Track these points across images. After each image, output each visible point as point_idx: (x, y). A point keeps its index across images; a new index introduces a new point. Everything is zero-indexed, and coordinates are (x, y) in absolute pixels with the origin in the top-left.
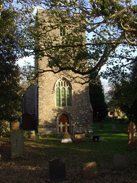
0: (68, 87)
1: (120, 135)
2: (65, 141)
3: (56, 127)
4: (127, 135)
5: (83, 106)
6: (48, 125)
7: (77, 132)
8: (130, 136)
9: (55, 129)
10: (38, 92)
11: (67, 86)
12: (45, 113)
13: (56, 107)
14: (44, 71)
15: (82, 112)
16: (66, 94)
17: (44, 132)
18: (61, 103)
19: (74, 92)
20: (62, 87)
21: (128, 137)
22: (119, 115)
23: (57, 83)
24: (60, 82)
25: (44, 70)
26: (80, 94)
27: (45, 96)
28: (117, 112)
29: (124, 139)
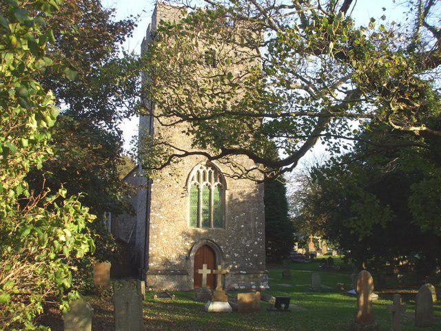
0: (217, 183)
1: (331, 296)
2: (216, 306)
3: (187, 274)
4: (356, 299)
5: (250, 229)
6: (170, 270)
7: (234, 288)
8: (362, 299)
9: (185, 278)
10: (149, 193)
11: (216, 181)
12: (164, 240)
13: (190, 229)
14: (187, 154)
15: (246, 241)
16: (213, 198)
17: (161, 284)
18: (201, 219)
19: (231, 197)
20: (205, 183)
21: (358, 301)
22: (318, 249)
23: (194, 174)
24: (201, 171)
25: (186, 152)
26: (244, 202)
27: (166, 203)
28: (315, 241)
29: (341, 305)
